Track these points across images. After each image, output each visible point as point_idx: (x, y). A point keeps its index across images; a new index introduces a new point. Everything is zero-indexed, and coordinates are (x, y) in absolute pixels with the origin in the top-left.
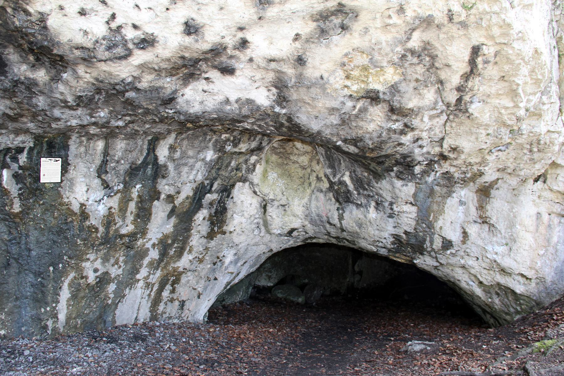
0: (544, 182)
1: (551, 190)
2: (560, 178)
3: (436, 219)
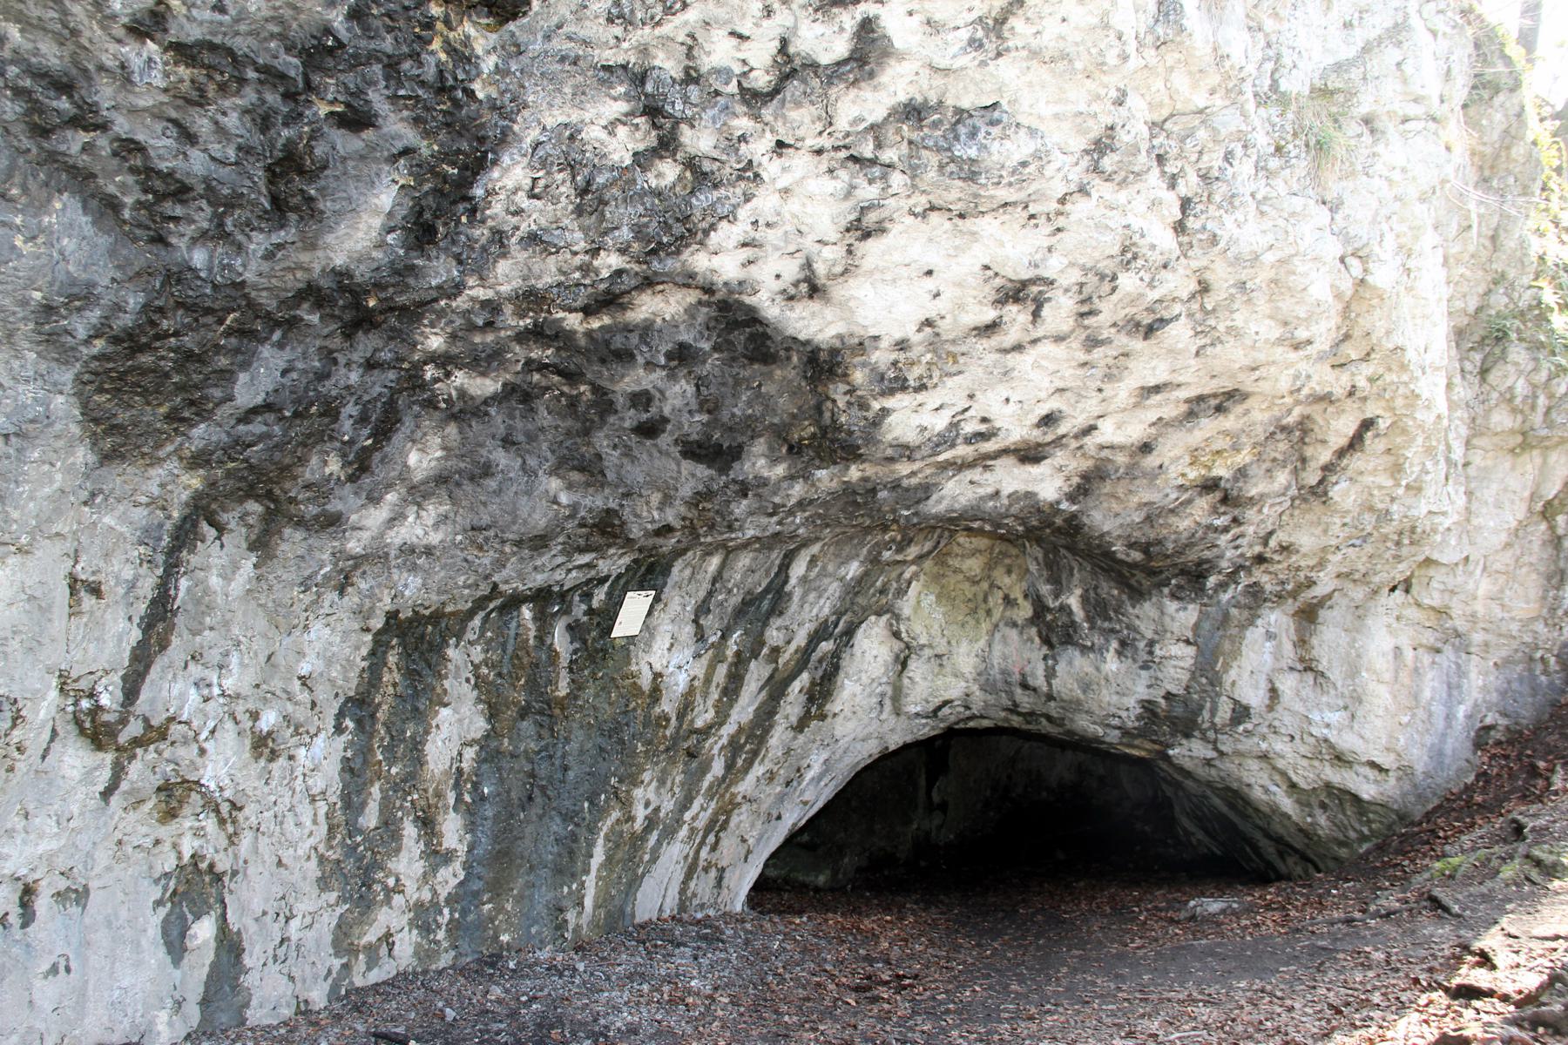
0: (1407, 591)
1: (1419, 605)
2: (1434, 584)
3: (1227, 667)
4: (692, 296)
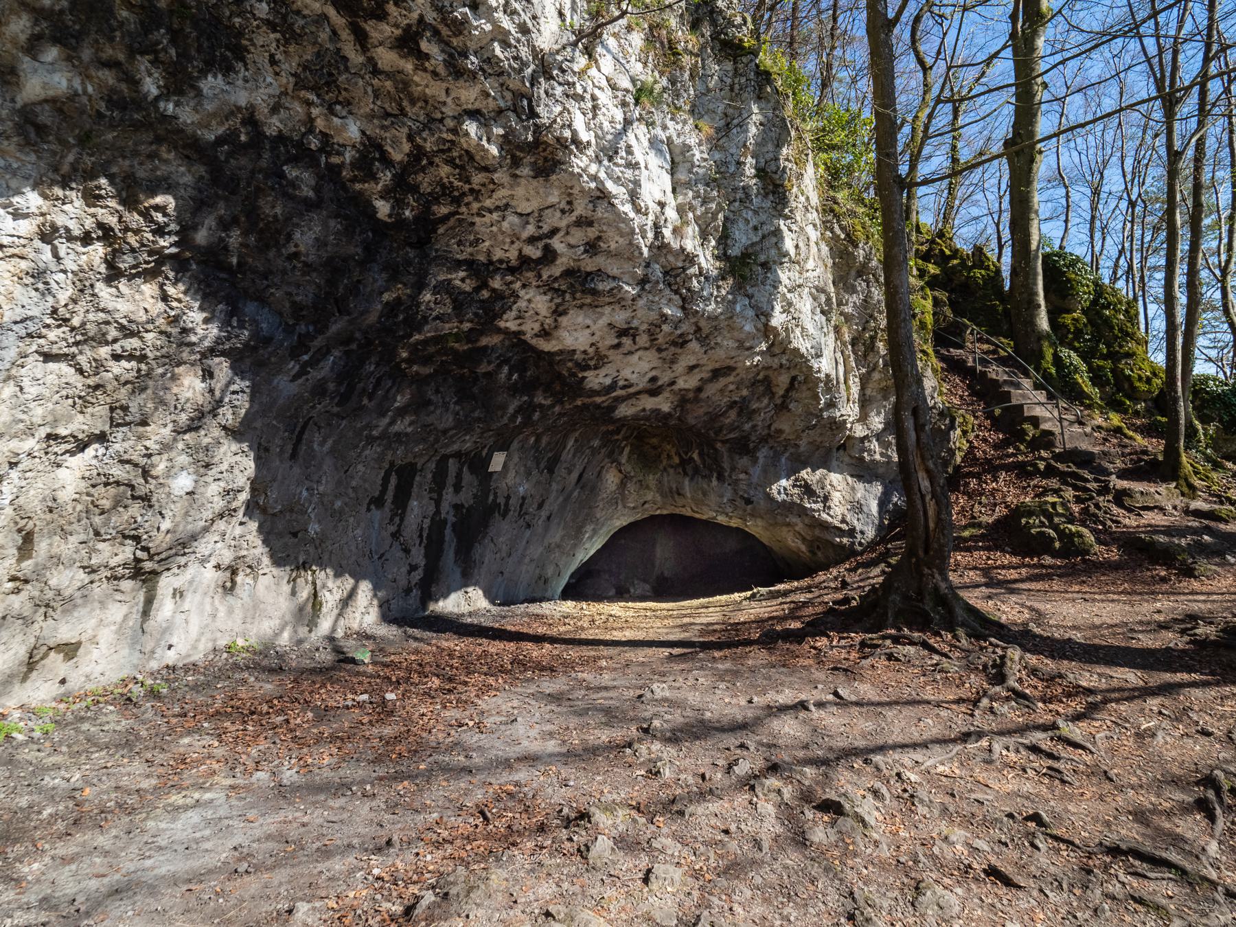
4: (501, 337)
